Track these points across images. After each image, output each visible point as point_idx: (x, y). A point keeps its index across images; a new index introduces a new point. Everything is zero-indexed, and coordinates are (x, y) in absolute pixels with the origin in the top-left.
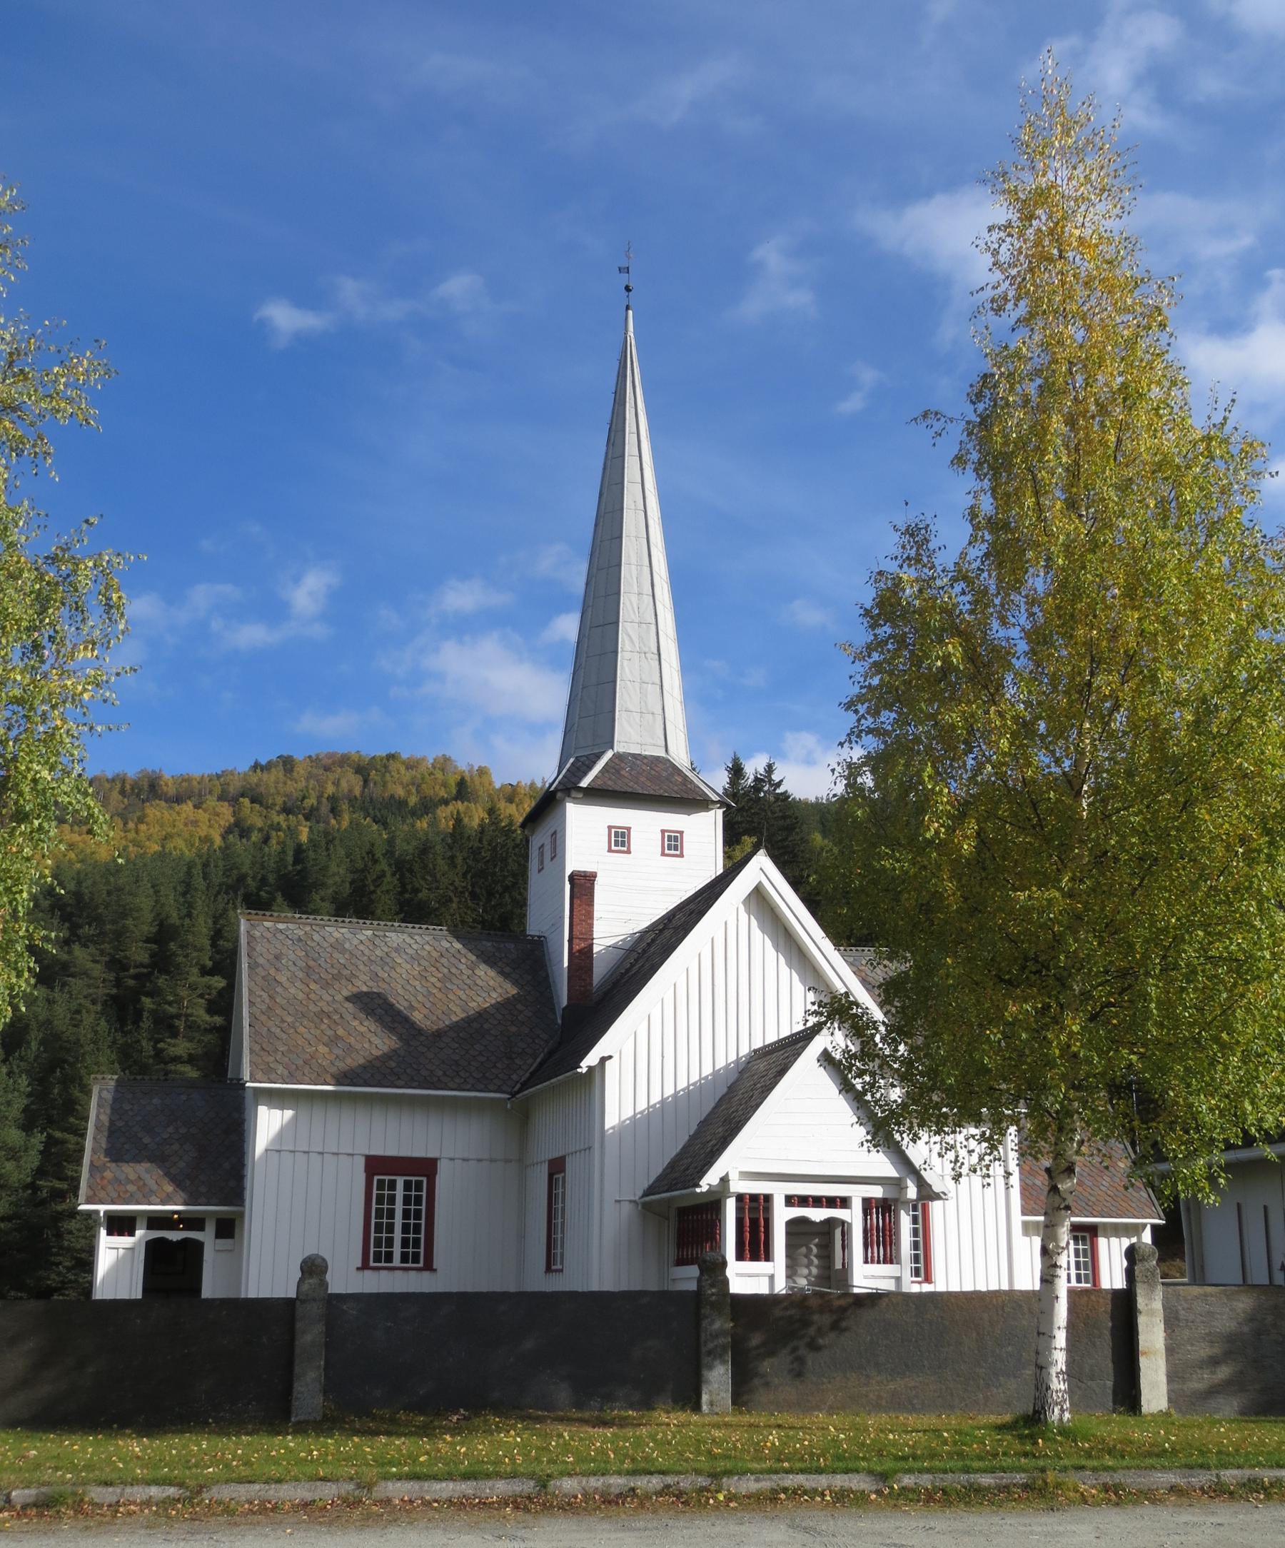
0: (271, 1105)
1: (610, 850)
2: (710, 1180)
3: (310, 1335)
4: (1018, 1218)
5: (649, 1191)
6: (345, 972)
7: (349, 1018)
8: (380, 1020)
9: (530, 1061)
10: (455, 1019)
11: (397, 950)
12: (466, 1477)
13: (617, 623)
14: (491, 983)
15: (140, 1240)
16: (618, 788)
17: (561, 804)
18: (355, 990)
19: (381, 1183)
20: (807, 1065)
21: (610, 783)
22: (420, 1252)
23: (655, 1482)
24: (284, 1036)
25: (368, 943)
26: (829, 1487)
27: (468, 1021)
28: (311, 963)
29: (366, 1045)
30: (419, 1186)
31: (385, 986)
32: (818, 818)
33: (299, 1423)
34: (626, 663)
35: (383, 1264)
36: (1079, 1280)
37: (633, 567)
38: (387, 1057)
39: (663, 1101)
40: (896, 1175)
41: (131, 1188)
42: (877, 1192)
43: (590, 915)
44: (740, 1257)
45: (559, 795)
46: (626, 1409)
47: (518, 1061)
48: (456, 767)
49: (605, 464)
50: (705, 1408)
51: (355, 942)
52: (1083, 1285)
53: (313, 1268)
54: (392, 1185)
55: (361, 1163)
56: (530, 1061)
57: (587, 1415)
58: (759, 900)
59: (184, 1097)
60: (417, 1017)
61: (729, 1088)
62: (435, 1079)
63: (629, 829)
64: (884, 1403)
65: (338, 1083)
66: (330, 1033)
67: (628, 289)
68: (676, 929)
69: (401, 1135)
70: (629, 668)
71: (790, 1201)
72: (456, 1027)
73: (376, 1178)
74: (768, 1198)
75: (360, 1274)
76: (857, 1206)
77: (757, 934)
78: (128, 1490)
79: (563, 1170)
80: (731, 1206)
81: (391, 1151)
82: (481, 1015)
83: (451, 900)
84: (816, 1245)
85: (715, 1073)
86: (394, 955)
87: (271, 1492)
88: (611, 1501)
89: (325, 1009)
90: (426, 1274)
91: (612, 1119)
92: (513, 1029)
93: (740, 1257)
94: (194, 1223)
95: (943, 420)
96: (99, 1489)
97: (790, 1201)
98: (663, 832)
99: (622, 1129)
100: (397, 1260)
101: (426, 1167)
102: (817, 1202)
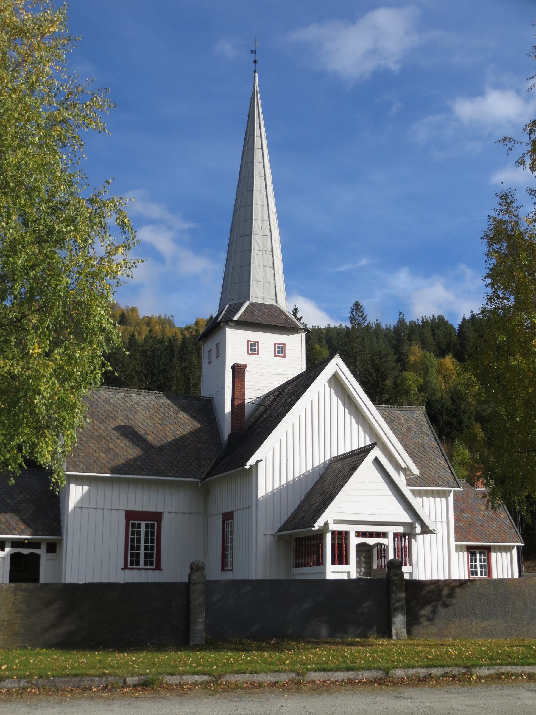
0: (77, 484)
1: (248, 353)
2: (319, 523)
3: (197, 600)
4: (453, 543)
5: (281, 529)
6: (112, 415)
7: (115, 439)
8: (131, 440)
9: (209, 462)
10: (169, 440)
11: (137, 404)
12: (348, 669)
13: (251, 235)
14: (187, 421)
15: (7, 554)
16: (253, 321)
17: (223, 329)
18: (117, 424)
19: (133, 525)
20: (367, 463)
21: (249, 318)
22: (154, 561)
23: (440, 671)
24: (82, 448)
25: (122, 400)
26: (523, 672)
27: (176, 441)
28: (94, 410)
29: (125, 453)
30: (153, 526)
31: (133, 422)
32: (317, 337)
33: (194, 645)
34: (255, 256)
35: (135, 567)
36: (481, 574)
37: (259, 206)
38: (135, 460)
39: (287, 483)
40: (411, 521)
41: (3, 526)
42: (400, 530)
43: (243, 387)
44: (333, 563)
45: (222, 324)
46: (354, 637)
47: (203, 462)
48: (120, 307)
49: (243, 152)
50: (394, 637)
51: (116, 399)
52: (484, 576)
53: (196, 568)
54: (139, 526)
55: (123, 515)
56: (209, 462)
57: (337, 640)
58: (336, 381)
59: (27, 479)
60: (150, 438)
61: (321, 477)
62: (161, 471)
63: (258, 342)
64: (479, 633)
65: (112, 473)
66: (106, 446)
67: (255, 62)
68: (289, 395)
69: (143, 500)
70: (257, 258)
71: (359, 534)
72: (170, 444)
73: (131, 522)
74: (347, 533)
75: (123, 571)
76: (391, 536)
77: (334, 398)
78: (184, 677)
79: (232, 518)
80: (329, 536)
81: (139, 508)
82: (183, 438)
83: (134, 377)
84: (364, 557)
85: (314, 469)
86: (136, 406)
87: (255, 678)
88: (423, 680)
89: (103, 434)
90: (157, 572)
91: (261, 493)
92: (199, 445)
93: (333, 563)
94: (35, 544)
95: (513, 142)
96: (169, 677)
97: (359, 534)
98: (275, 344)
99: (267, 497)
100: (142, 565)
101: (157, 517)
102: (371, 535)
